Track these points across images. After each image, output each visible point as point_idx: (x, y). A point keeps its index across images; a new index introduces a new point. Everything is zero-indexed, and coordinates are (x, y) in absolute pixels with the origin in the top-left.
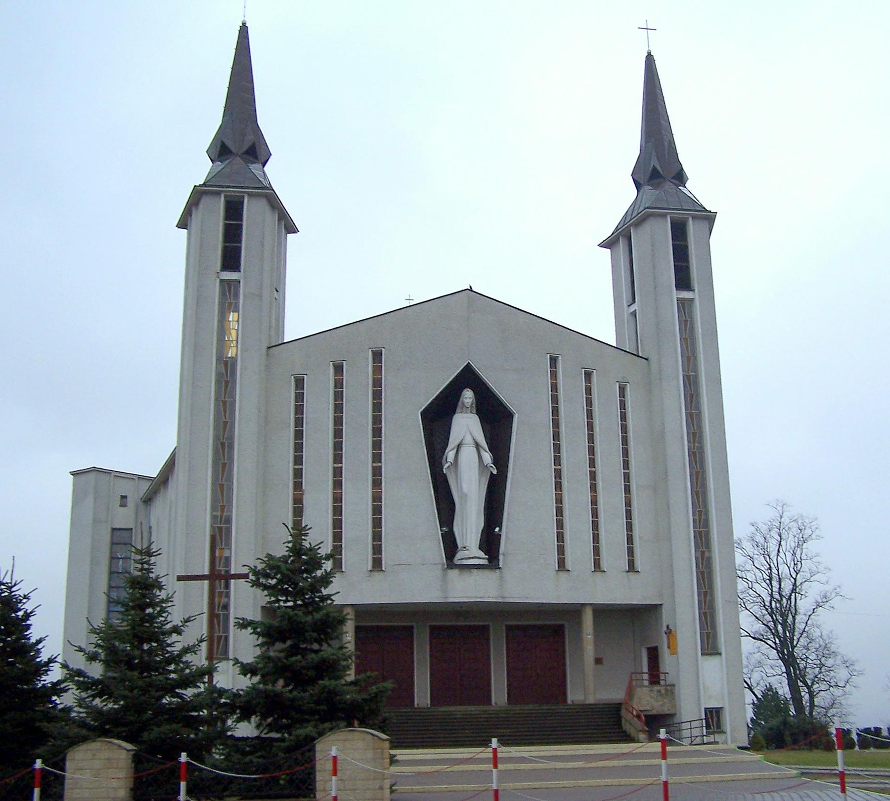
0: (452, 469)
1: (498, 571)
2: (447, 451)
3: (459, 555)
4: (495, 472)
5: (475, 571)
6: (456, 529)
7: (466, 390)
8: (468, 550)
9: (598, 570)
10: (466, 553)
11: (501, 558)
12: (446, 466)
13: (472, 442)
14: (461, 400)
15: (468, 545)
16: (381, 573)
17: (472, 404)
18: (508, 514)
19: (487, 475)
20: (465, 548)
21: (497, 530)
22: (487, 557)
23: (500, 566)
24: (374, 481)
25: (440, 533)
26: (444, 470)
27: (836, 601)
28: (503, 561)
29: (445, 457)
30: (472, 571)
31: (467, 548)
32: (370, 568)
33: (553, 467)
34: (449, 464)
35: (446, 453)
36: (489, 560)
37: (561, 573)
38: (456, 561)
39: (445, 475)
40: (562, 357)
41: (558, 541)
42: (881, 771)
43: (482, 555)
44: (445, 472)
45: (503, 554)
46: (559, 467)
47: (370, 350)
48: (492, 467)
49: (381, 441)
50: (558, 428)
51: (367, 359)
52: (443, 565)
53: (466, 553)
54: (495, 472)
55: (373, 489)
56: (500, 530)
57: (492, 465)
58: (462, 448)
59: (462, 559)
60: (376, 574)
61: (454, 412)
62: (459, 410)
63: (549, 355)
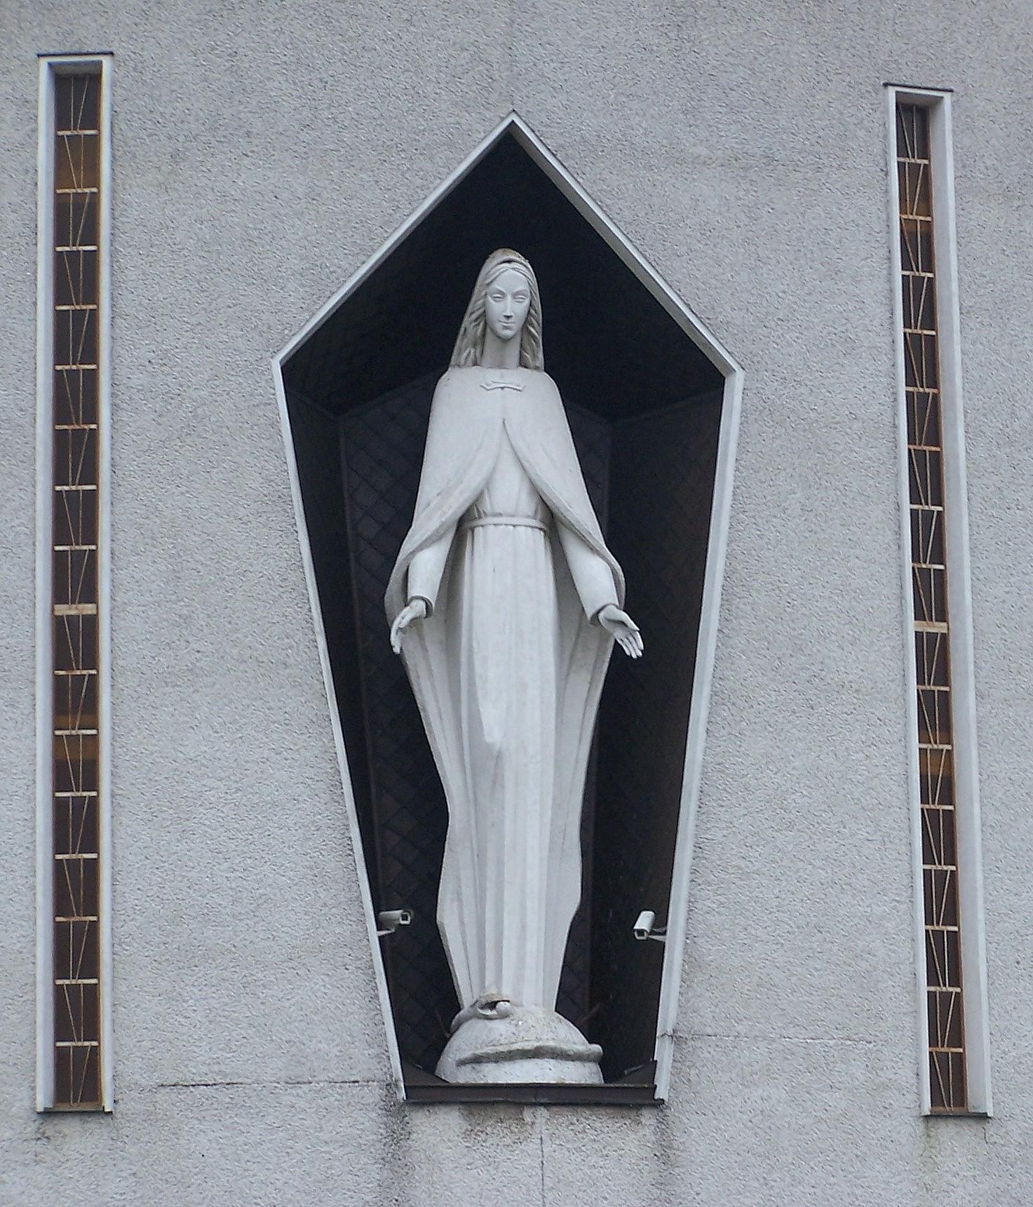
0: (432, 632)
1: (648, 1117)
2: (407, 547)
3: (466, 1040)
4: (635, 648)
5: (539, 1118)
6: (449, 916)
7: (500, 255)
8: (504, 1016)
9: (957, 1110)
10: (499, 1034)
11: (664, 1052)
12: (403, 618)
13: (527, 505)
14: (474, 305)
15: (506, 992)
16: (93, 1124)
17: (525, 328)
18: (698, 846)
19: (598, 661)
20: (493, 1005)
21: (644, 921)
22: (597, 1048)
23: (661, 1093)
24: (59, 686)
25: (374, 934)
26: (395, 640)
27: (990, 1128)
28: (676, 1071)
29: (396, 575)
30: (528, 1115)
31: (501, 1005)
32: (43, 1099)
33: (912, 626)
34: (418, 608)
35: (401, 557)
36: (606, 1064)
37: (947, 1131)
38: (452, 1068)
39: (398, 663)
40: (954, 104)
41: (932, 979)
42: (522, 938)
43: (570, 1037)
44: (397, 650)
45: (675, 1037)
46: (939, 628)
47: (44, 63)
48: (623, 623)
49: (92, 497)
50: (935, 438)
51: (29, 103)
52: (390, 1086)
53: (499, 1034)
54: (635, 648)
55: (57, 727)
56: (661, 922)
57: (625, 617)
58: (479, 531)
59: (477, 1060)
60: (70, 1127)
61: (439, 362)
62: (463, 349)
63: (892, 92)
